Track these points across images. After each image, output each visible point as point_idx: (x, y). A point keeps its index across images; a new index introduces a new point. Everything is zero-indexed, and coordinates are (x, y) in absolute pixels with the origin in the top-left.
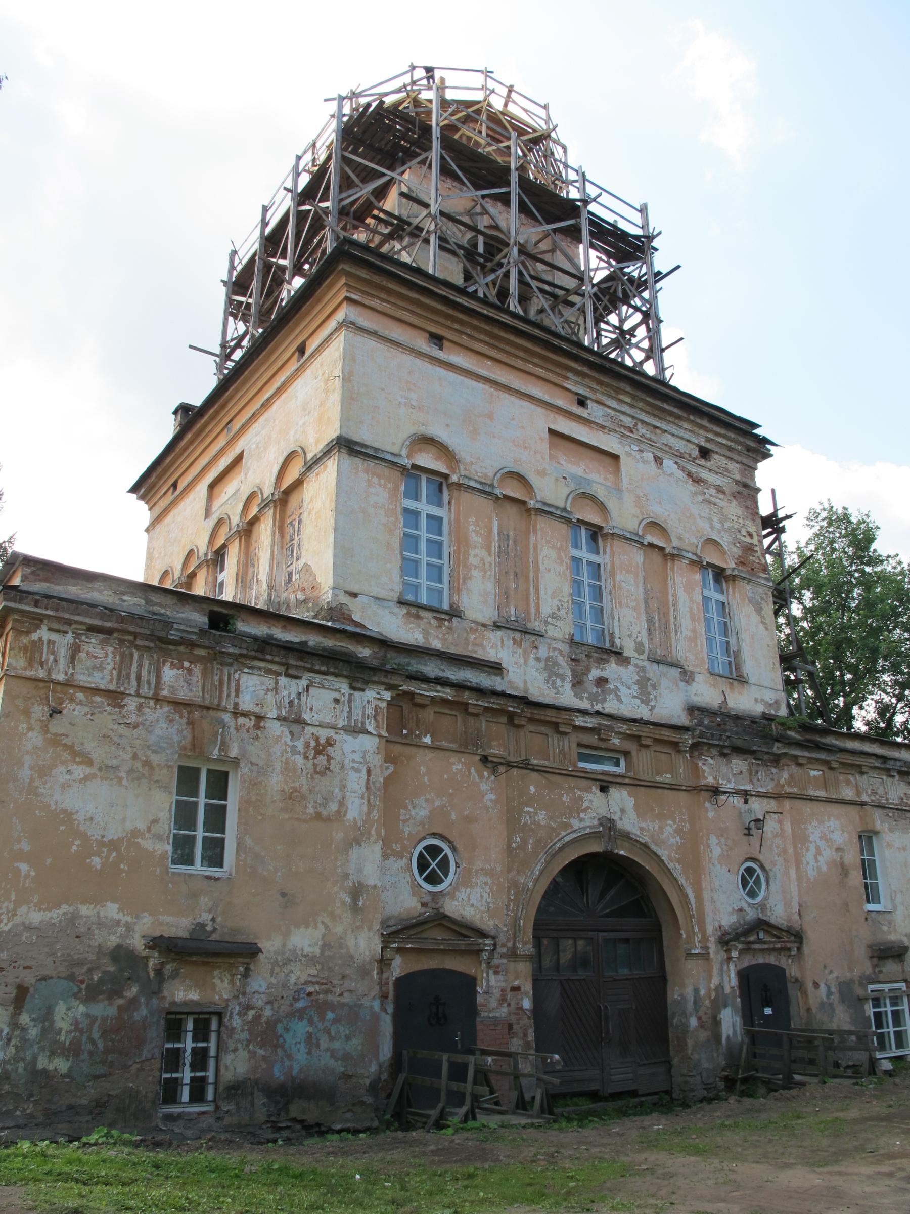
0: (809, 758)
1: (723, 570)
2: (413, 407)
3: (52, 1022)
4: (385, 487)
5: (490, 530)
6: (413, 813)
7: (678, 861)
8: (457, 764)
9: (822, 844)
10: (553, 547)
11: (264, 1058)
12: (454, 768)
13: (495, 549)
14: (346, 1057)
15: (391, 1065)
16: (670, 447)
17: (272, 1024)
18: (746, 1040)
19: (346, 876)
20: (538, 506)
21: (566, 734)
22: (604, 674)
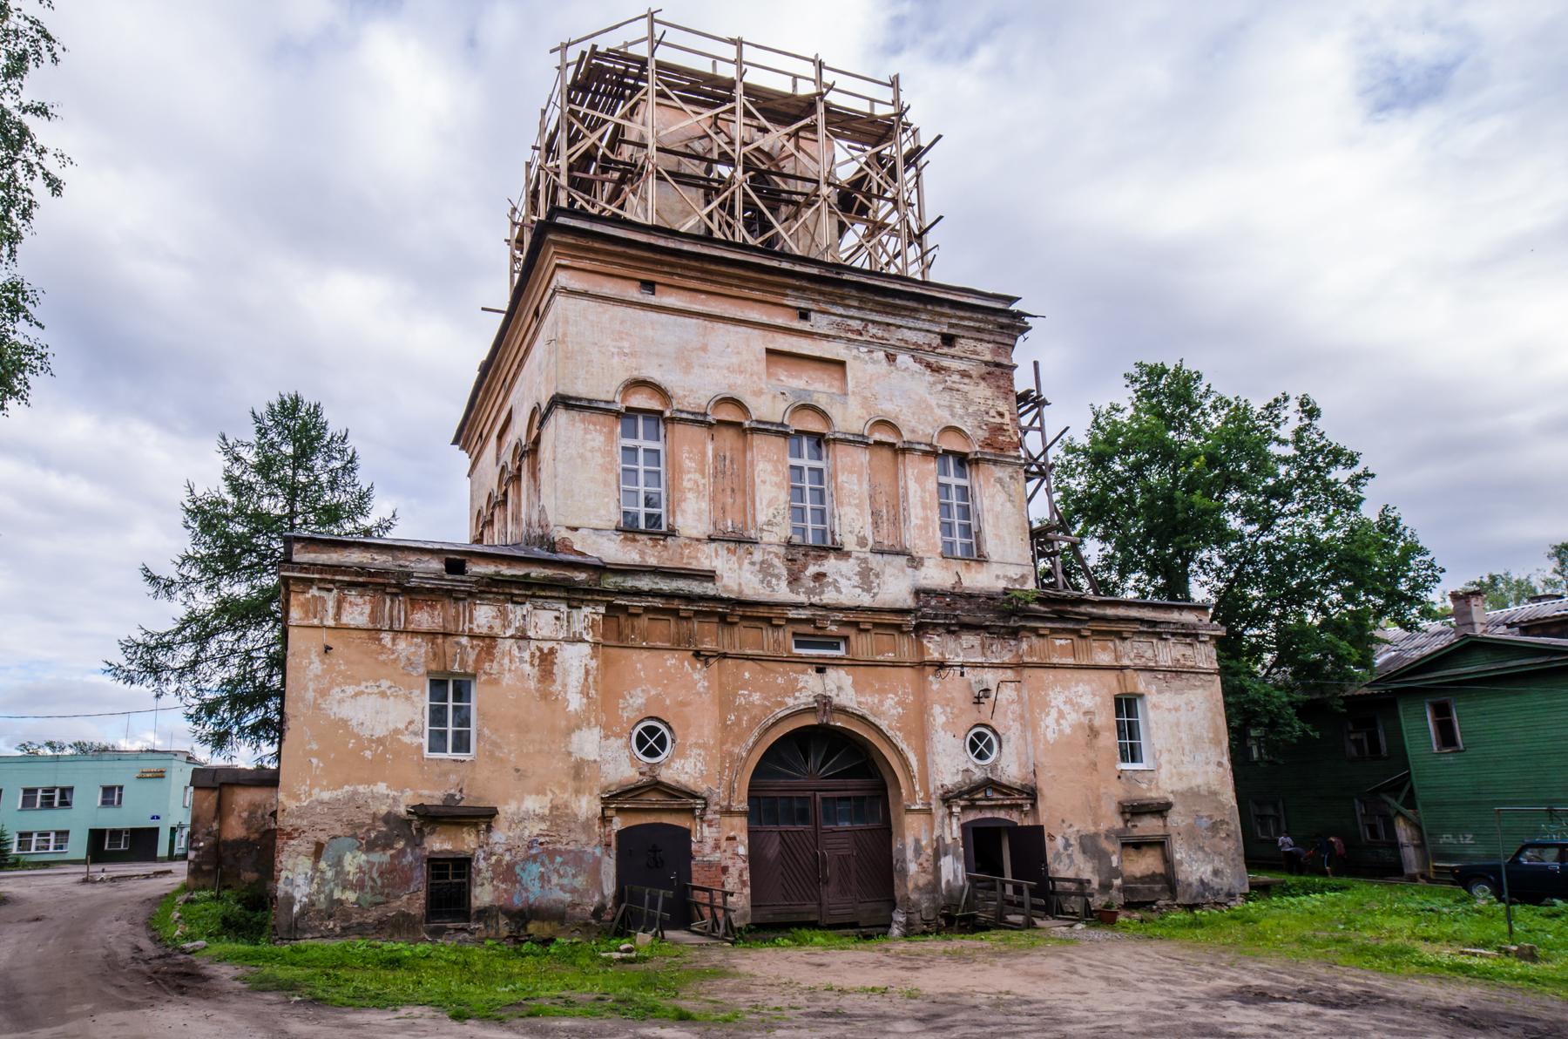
0: (1051, 629)
1: (966, 454)
2: (626, 355)
3: (343, 867)
4: (601, 432)
5: (704, 454)
6: (631, 701)
7: (899, 729)
8: (671, 660)
9: (1066, 709)
10: (769, 461)
11: (506, 891)
12: (668, 663)
13: (709, 469)
14: (573, 891)
15: (615, 897)
16: (906, 342)
17: (510, 867)
18: (967, 884)
19: (570, 754)
20: (754, 425)
21: (781, 626)
22: (822, 570)
